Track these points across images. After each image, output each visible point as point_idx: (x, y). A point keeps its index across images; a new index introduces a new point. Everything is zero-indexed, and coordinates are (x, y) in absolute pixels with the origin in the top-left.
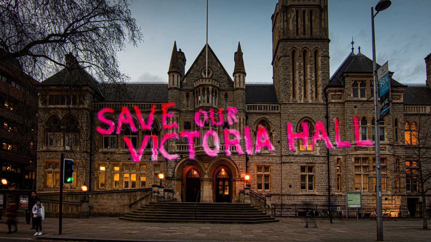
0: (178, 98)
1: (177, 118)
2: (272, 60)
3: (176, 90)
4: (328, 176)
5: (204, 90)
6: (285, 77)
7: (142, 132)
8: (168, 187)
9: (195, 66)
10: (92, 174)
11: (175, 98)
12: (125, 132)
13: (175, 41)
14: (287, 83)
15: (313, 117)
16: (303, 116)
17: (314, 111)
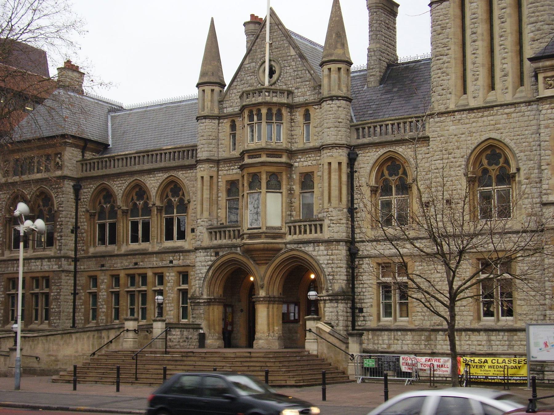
0: (214, 134)
1: (211, 177)
2: (244, 52)
3: (207, 121)
4: (77, 314)
5: (251, 112)
6: (438, 50)
7: (157, 210)
8: (193, 317)
9: (247, 62)
10: (77, 297)
11: (205, 138)
12: (132, 210)
13: (212, 19)
14: (444, 63)
15: (506, 136)
16: (483, 138)
17: (511, 120)
